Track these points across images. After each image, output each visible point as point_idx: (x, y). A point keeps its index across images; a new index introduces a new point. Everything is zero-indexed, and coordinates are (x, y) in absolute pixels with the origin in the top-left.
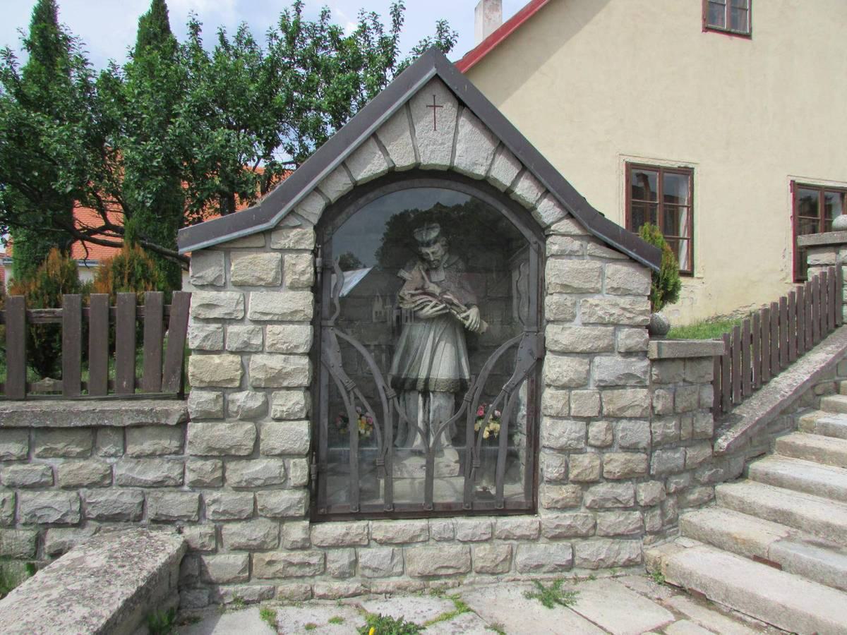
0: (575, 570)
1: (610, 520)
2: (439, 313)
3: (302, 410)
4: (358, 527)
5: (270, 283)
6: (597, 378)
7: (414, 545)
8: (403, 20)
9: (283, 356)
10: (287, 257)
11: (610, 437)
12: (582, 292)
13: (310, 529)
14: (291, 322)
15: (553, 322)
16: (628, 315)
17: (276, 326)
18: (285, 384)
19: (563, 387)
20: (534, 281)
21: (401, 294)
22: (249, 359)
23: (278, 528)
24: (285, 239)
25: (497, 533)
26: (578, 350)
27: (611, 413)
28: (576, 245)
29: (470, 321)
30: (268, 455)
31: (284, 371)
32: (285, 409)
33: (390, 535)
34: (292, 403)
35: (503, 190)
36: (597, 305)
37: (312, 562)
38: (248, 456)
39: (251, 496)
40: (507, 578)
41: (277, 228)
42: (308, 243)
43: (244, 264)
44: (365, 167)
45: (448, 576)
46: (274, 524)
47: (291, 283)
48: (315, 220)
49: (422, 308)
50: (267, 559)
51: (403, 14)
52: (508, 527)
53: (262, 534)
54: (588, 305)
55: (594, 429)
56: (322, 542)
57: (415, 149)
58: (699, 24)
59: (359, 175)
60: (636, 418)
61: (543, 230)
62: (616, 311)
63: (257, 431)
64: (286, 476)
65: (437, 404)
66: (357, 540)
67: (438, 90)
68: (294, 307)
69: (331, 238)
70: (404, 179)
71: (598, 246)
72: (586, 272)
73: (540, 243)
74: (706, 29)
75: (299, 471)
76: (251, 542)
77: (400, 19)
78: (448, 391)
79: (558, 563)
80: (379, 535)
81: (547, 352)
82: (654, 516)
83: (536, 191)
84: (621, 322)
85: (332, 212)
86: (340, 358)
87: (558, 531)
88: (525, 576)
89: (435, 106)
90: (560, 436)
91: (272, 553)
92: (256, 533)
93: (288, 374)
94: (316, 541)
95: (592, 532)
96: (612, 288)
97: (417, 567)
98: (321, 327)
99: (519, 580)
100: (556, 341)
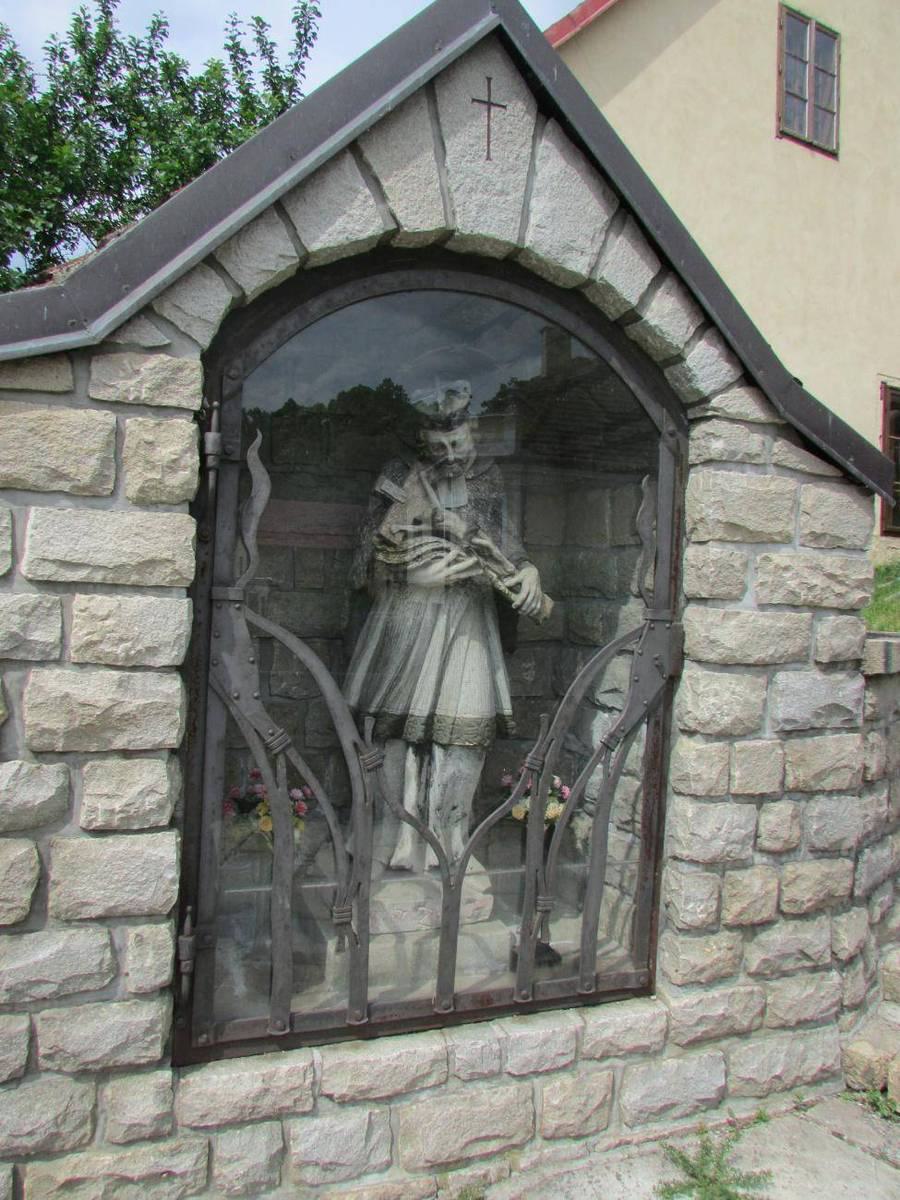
0: (729, 1104)
1: (795, 994)
2: (463, 576)
3: (161, 807)
4: (290, 1073)
5: (84, 488)
6: (780, 716)
7: (413, 1097)
8: (314, 34)
9: (116, 674)
10: (131, 423)
11: (796, 832)
12: (760, 540)
13: (174, 1087)
14: (138, 588)
15: (702, 600)
16: (838, 589)
17: (99, 598)
18: (120, 742)
19: (721, 736)
20: (666, 514)
21: (384, 530)
22: (23, 681)
23: (92, 1094)
24: (130, 378)
25: (586, 1048)
26: (751, 661)
27: (801, 785)
28: (754, 442)
29: (522, 595)
30: (68, 921)
32: (117, 806)
33: (364, 1083)
34: (137, 789)
35: (613, 313)
36: (786, 569)
37: (176, 1170)
38: (14, 925)
39: (21, 1023)
40: (606, 1142)
41: (104, 348)
42: (187, 392)
43: (13, 433)
44: (331, 223)
45: (487, 1157)
46: (81, 1087)
47: (142, 490)
48: (205, 337)
49: (427, 565)
50: (62, 1178)
51: (319, 25)
52: (608, 1033)
53: (50, 1115)
54: (771, 567)
55: (771, 817)
56: (203, 1117)
57: (445, 194)
58: (771, 124)
59: (315, 239)
60: (840, 792)
61: (685, 407)
62: (817, 580)
63: (41, 861)
64: (116, 970)
65: (451, 770)
66: (288, 1102)
67: (497, 70)
68: (148, 549)
69: (240, 389)
70: (411, 266)
71: (793, 447)
72: (772, 500)
73: (680, 435)
74: (782, 134)
75: (150, 955)
76: (17, 1142)
77: (309, 34)
78: (480, 744)
79: (702, 1097)
80: (338, 1086)
81: (687, 662)
82: (856, 975)
83: (686, 322)
84: (825, 604)
85: (249, 323)
86: (255, 677)
87: (701, 1029)
88: (638, 1133)
90: (714, 837)
91: (74, 1158)
92: (34, 1116)
93: (129, 719)
94: (187, 1117)
95: (757, 1022)
96: (813, 533)
97: (426, 1146)
98: (211, 601)
99: (628, 1143)
100: (712, 642)
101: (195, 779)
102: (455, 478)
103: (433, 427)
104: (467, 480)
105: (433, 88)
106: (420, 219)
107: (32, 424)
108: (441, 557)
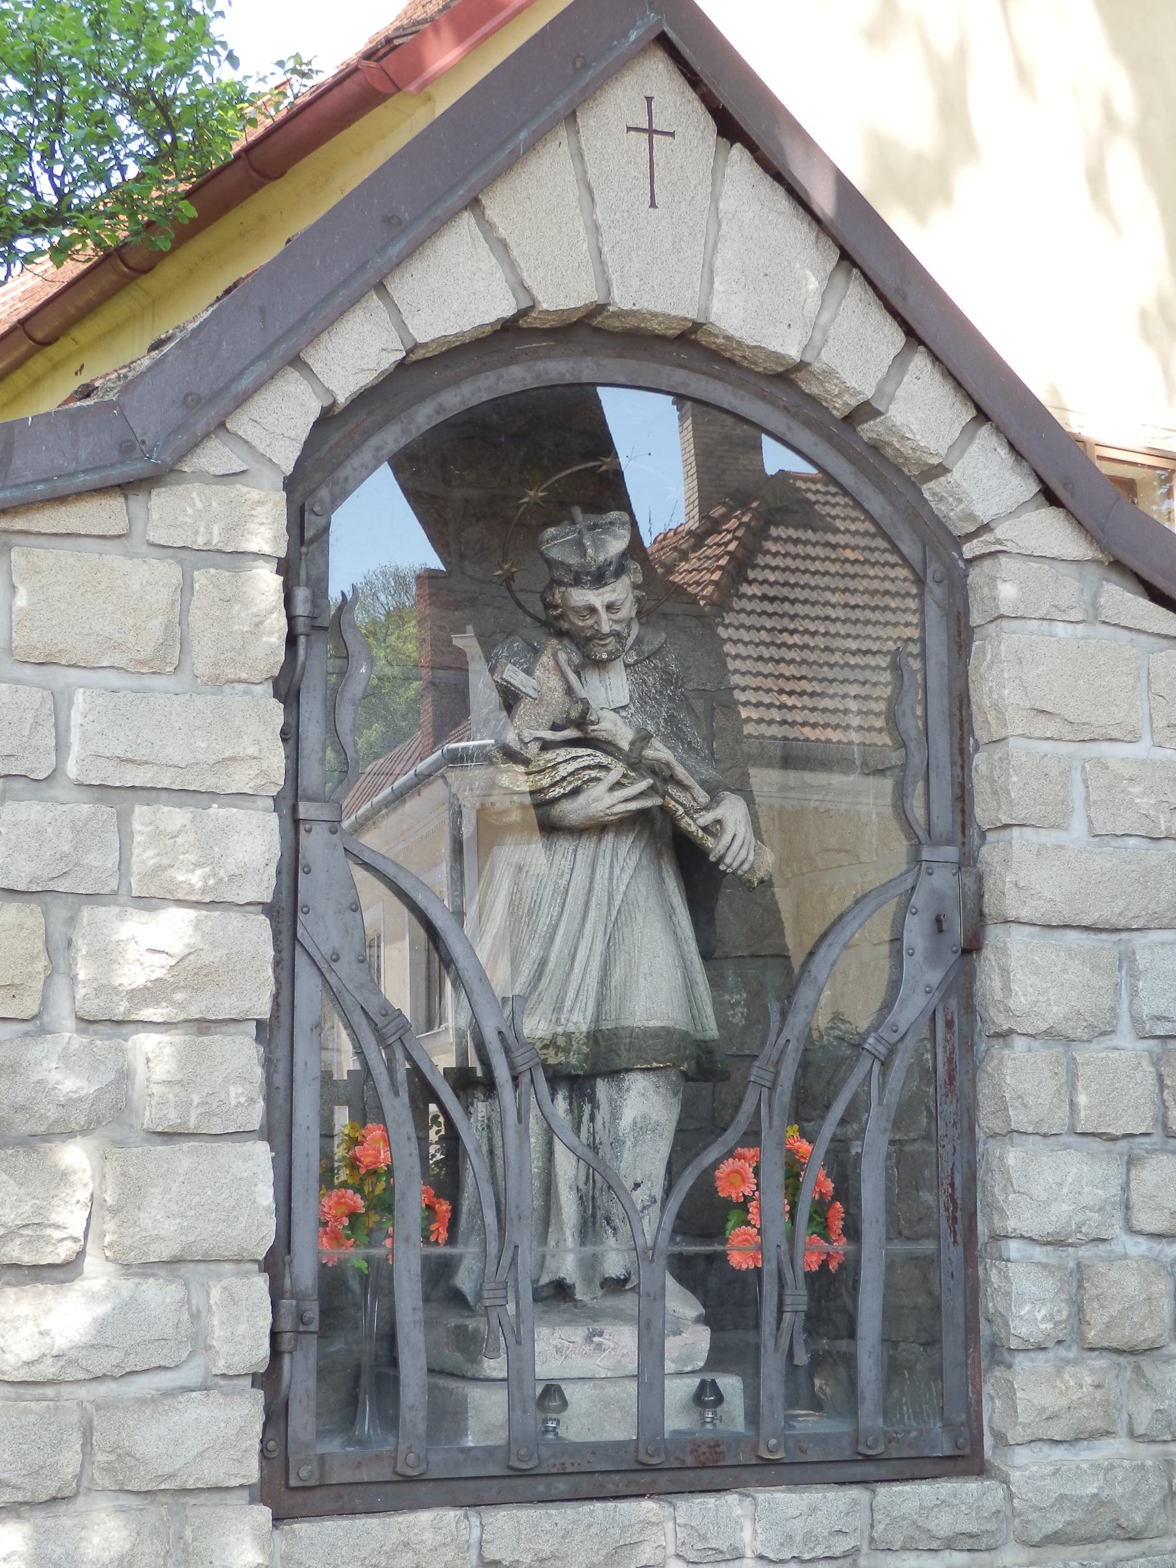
2: (633, 806)
20: (939, 704)
29: (726, 839)
48: (287, 456)
49: (576, 792)
101: (280, 1080)
102: (610, 660)
103: (577, 582)
104: (627, 666)
105: (575, 121)
106: (561, 292)
108: (598, 780)
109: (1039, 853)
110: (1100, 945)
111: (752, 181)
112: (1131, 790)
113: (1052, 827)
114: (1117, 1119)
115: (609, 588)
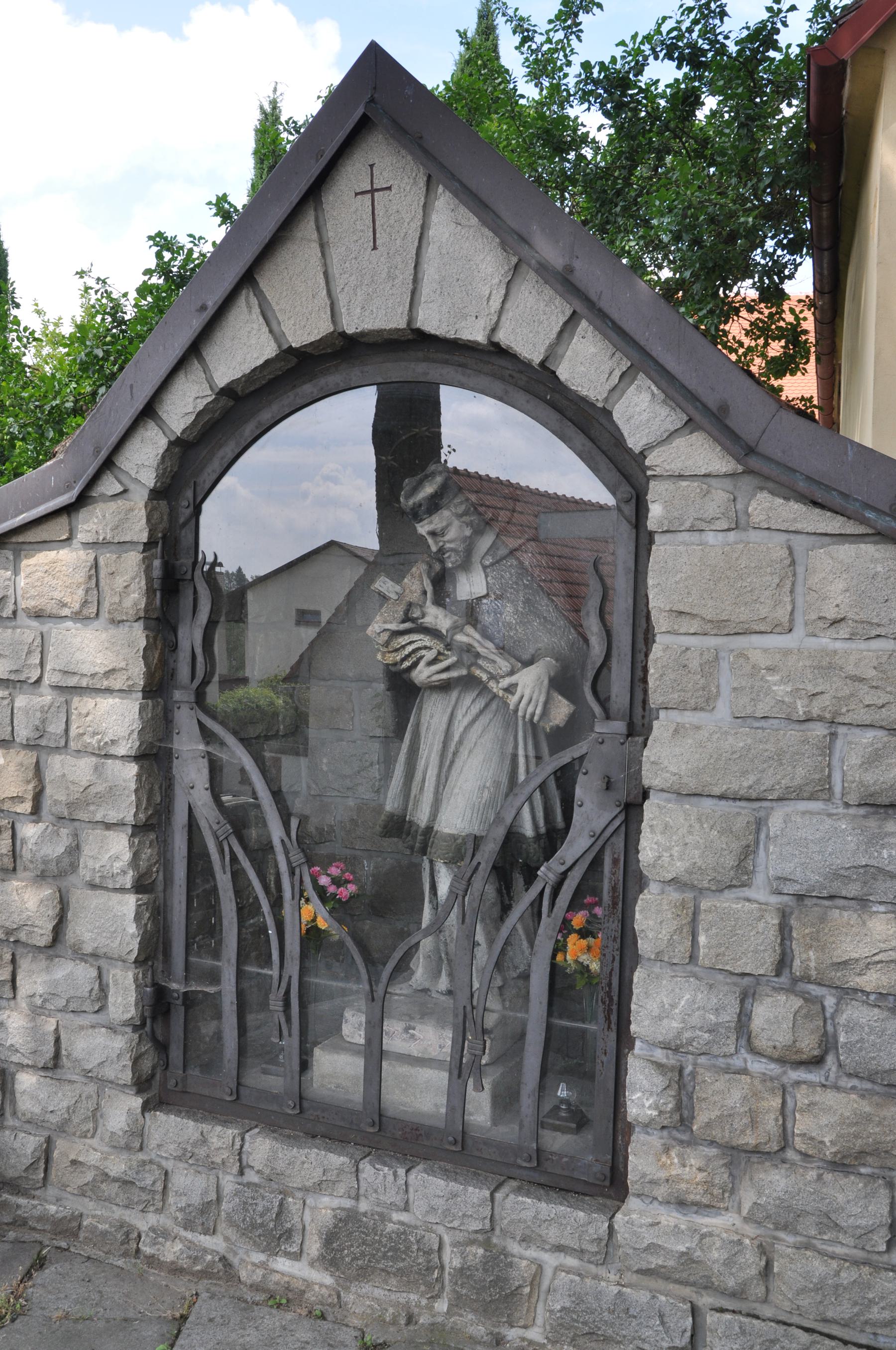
31: (93, 790)
53: (65, 1104)
89: (373, 191)
104: (485, 568)
106: (305, 328)
107: (47, 567)
109: (676, 731)
110: (738, 810)
111: (452, 207)
112: (769, 678)
113: (695, 709)
114: (736, 960)
115: (426, 522)
